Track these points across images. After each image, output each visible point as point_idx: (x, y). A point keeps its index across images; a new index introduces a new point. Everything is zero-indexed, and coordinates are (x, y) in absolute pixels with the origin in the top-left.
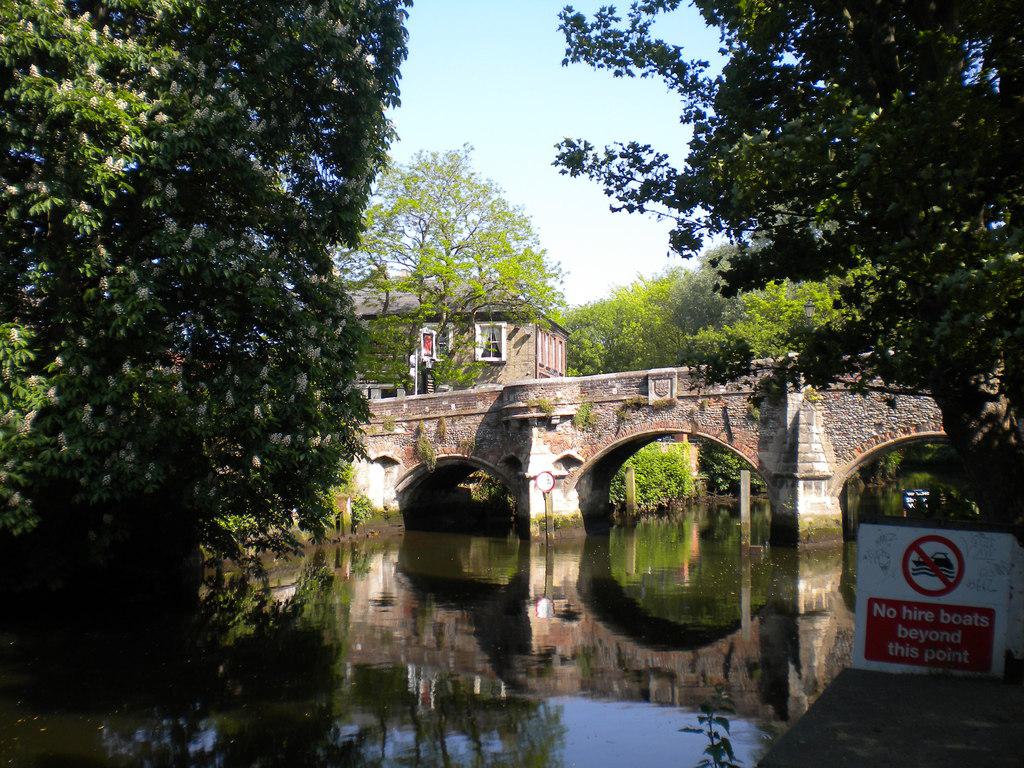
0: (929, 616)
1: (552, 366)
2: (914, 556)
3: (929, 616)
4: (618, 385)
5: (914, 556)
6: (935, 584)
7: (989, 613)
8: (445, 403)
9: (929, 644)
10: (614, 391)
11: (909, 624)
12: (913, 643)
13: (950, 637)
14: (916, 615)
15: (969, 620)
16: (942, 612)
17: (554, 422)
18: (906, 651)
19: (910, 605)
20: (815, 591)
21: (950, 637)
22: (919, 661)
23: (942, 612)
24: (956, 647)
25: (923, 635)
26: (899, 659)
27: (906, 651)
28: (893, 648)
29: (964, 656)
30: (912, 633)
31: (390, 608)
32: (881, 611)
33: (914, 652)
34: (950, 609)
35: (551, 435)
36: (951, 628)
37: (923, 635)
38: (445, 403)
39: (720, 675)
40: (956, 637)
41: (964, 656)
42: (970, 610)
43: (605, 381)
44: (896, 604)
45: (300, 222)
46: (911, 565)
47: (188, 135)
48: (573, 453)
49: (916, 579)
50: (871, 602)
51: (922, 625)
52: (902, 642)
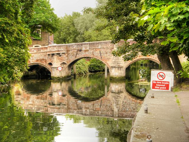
0: (161, 83)
1: (51, 40)
2: (159, 75)
3: (161, 83)
4: (75, 46)
5: (159, 75)
6: (161, 78)
7: (169, 82)
8: (33, 50)
9: (161, 86)
10: (74, 47)
11: (158, 84)
12: (159, 86)
13: (163, 85)
14: (159, 83)
15: (166, 83)
16: (162, 82)
17: (60, 54)
18: (157, 88)
19: (158, 81)
20: (120, 88)
21: (163, 85)
22: (159, 89)
23: (162, 82)
24: (164, 87)
25: (160, 85)
26: (157, 89)
27: (157, 88)
28: (156, 87)
29: (165, 88)
30: (158, 85)
31: (20, 96)
32: (154, 82)
33: (159, 88)
34: (164, 82)
35: (60, 58)
36: (163, 84)
37: (160, 85)
38: (33, 50)
39: (99, 107)
40: (164, 85)
41: (165, 88)
42: (166, 82)
43: (72, 45)
44: (156, 81)
45: (164, 60)
46: (158, 76)
47: (148, 54)
48: (65, 62)
49: (159, 78)
50: (153, 81)
51: (160, 84)
52: (157, 86)
